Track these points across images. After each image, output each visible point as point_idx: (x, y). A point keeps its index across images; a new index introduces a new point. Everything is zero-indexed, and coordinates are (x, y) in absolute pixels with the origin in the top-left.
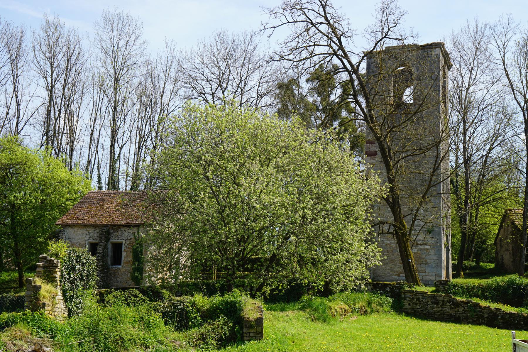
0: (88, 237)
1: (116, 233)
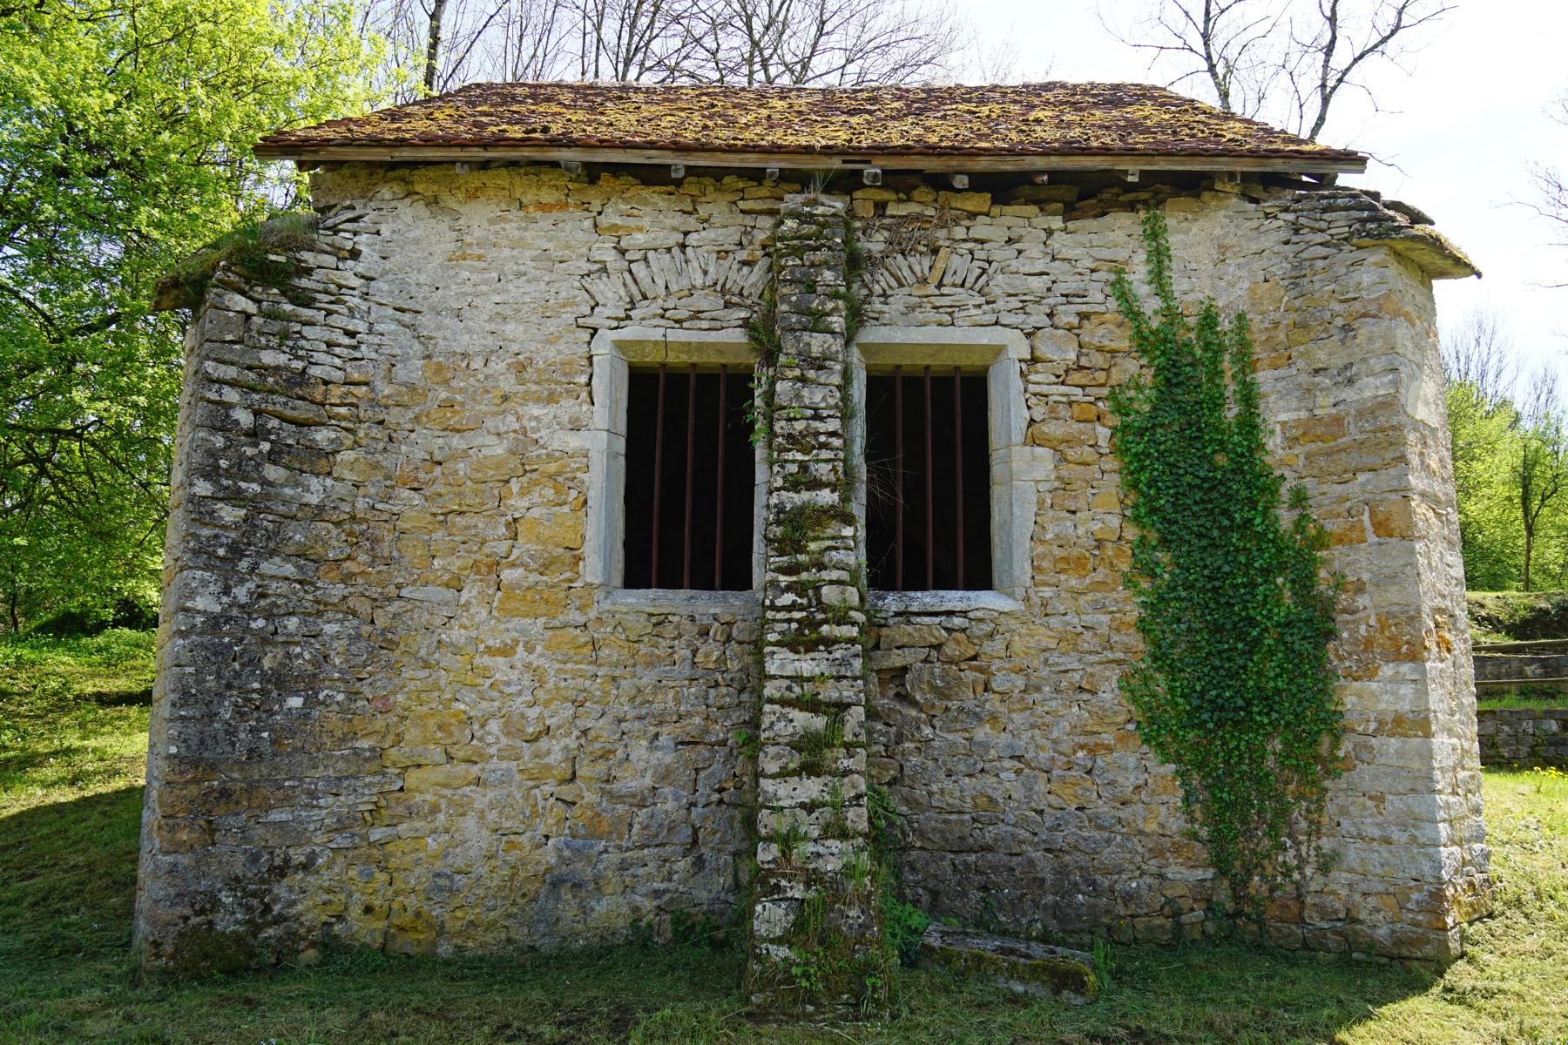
0: (610, 291)
1: (921, 264)
